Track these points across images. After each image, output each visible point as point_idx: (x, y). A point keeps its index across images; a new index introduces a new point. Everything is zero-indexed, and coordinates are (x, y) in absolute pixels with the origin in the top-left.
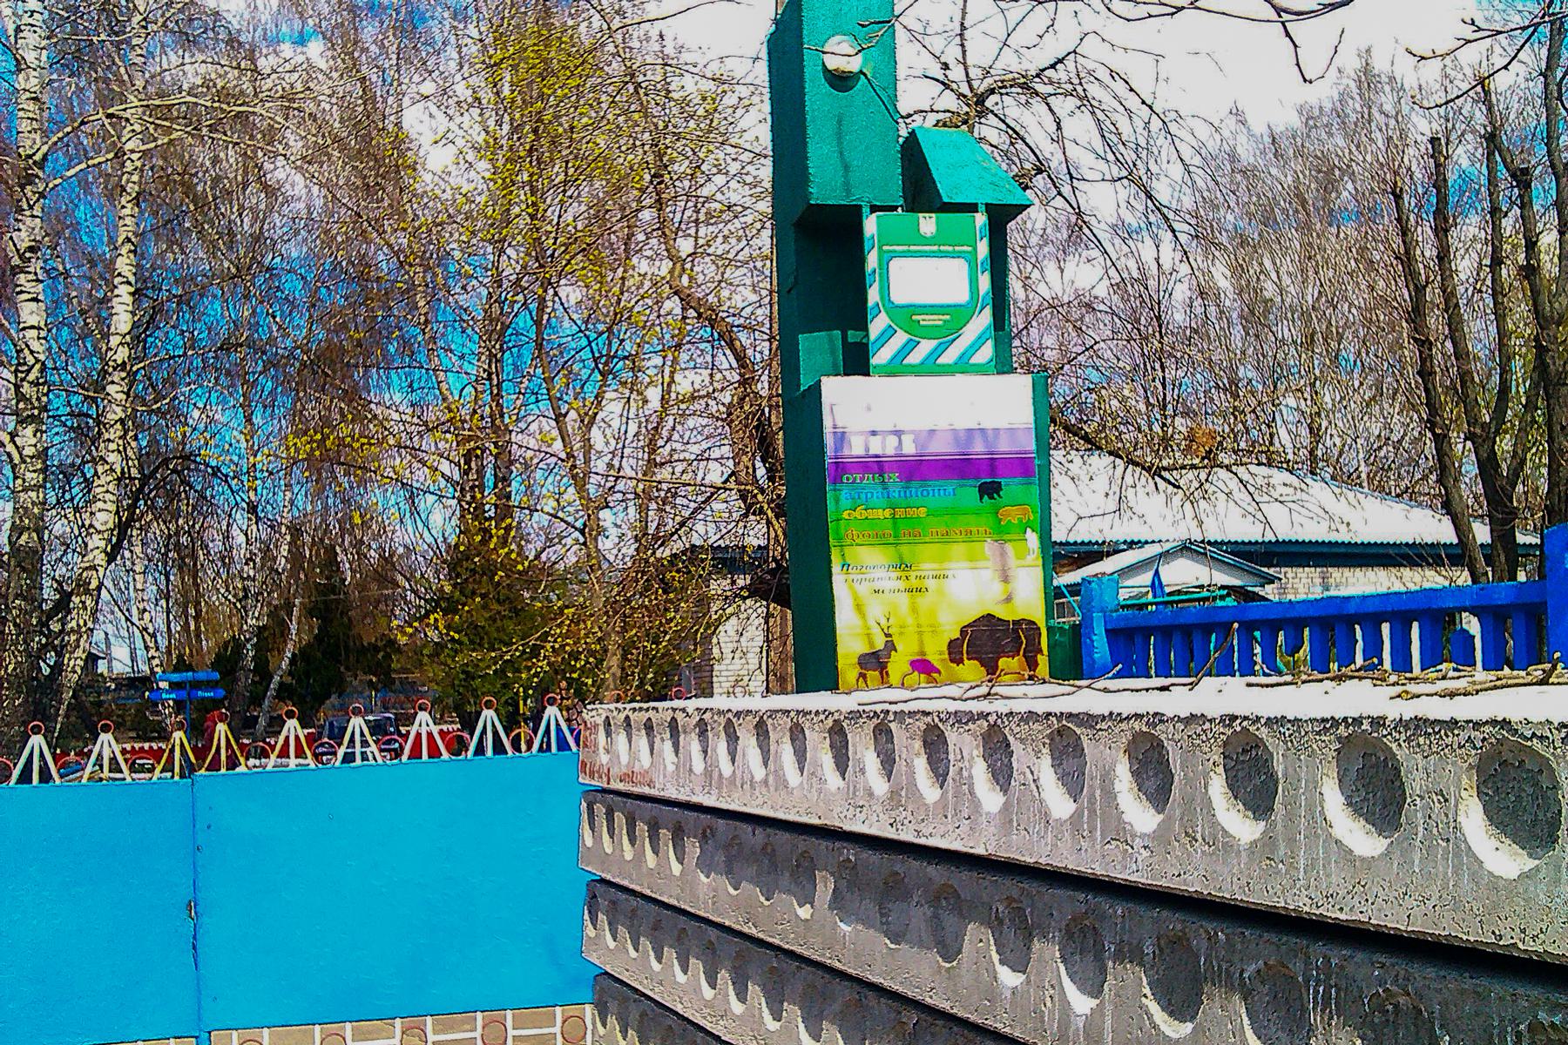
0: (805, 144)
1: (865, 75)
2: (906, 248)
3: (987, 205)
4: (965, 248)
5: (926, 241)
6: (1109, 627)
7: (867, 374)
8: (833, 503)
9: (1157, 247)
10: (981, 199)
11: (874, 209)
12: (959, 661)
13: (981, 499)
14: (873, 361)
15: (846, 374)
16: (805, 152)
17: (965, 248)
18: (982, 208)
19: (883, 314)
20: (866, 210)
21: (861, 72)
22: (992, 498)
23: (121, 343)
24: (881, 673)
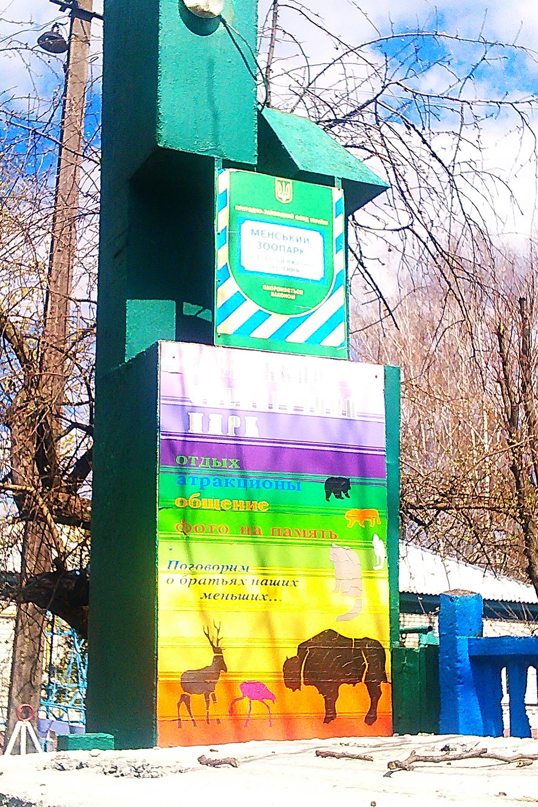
0: (156, 82)
1: (224, 22)
2: (260, 211)
3: (343, 180)
4: (322, 222)
5: (281, 207)
6: (473, 654)
7: (210, 342)
8: (443, 738)
9: (387, 242)
10: (340, 173)
11: (227, 164)
12: (295, 686)
13: (328, 496)
14: (220, 329)
15: (176, 341)
16: (156, 91)
17: (322, 222)
18: (338, 183)
19: (231, 280)
20: (218, 165)
21: (220, 16)
22: (339, 497)
23: (500, 294)
24: (207, 697)
